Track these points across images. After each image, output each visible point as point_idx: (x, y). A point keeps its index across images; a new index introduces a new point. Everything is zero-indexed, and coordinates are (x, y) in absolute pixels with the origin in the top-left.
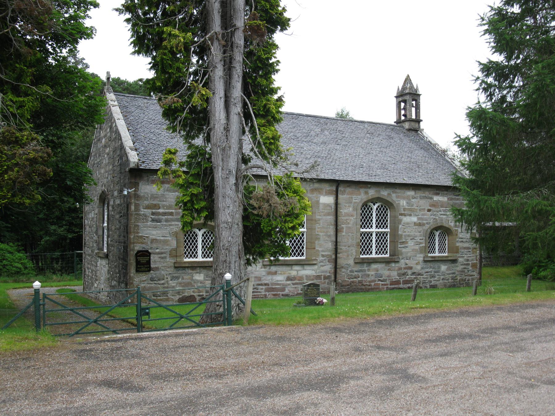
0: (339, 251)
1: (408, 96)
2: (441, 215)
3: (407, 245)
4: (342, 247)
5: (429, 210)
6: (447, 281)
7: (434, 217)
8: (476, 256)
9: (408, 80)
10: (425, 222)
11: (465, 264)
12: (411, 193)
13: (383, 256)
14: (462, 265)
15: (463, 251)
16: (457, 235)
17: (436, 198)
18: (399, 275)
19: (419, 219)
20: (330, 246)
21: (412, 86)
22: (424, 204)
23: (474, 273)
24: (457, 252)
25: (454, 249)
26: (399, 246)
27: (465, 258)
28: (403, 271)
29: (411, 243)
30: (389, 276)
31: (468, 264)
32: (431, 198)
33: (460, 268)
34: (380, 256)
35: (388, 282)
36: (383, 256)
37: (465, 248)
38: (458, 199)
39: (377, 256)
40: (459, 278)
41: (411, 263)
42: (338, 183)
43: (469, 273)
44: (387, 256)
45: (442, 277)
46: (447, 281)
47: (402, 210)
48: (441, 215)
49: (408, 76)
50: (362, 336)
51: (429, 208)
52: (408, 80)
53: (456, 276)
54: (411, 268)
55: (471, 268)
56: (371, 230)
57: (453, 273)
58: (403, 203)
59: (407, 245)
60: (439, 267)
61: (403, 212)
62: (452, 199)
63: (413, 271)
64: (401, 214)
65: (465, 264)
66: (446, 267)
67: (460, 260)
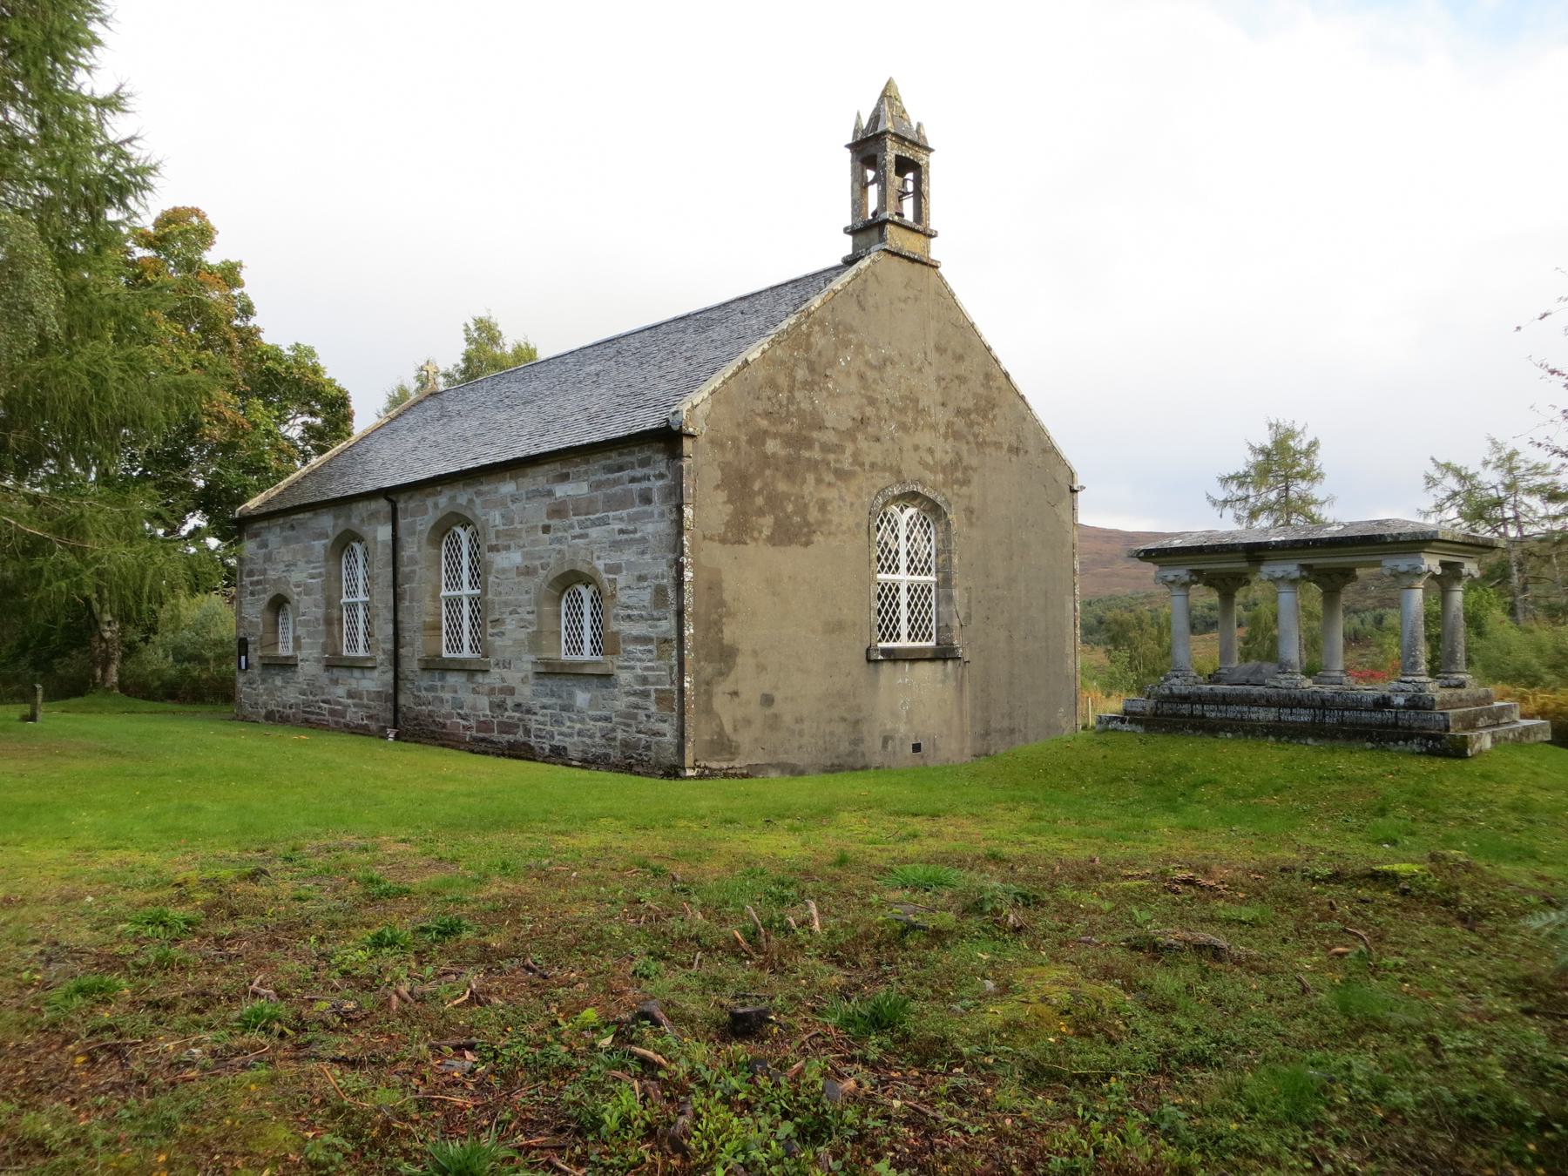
0: (402, 641)
1: (886, 153)
2: (574, 537)
3: (502, 629)
4: (406, 636)
5: (546, 529)
6: (588, 741)
7: (558, 547)
8: (671, 668)
9: (888, 95)
10: (537, 563)
11: (635, 694)
12: (508, 488)
13: (923, 644)
14: (628, 694)
15: (630, 648)
16: (613, 596)
17: (561, 491)
18: (492, 706)
19: (525, 556)
20: (390, 628)
21: (902, 115)
22: (536, 511)
23: (665, 727)
24: (615, 652)
25: (606, 643)
26: (490, 631)
27: (639, 672)
28: (497, 698)
29: (510, 624)
30: (474, 708)
31: (645, 694)
32: (550, 493)
33: (622, 703)
34: (917, 644)
35: (473, 723)
36: (923, 644)
37: (639, 640)
38: (616, 482)
39: (910, 644)
40: (620, 735)
41: (513, 677)
42: (390, 494)
43: (650, 725)
44: (932, 643)
45: (578, 726)
46: (588, 741)
47: (493, 536)
48: (574, 537)
49: (889, 84)
50: (1519, 868)
51: (547, 522)
52: (888, 95)
53: (614, 730)
54: (511, 691)
55: (653, 709)
56: (896, 577)
57: (607, 719)
58: (495, 517)
59: (502, 629)
60: (571, 695)
61: (494, 542)
62: (597, 486)
63: (517, 699)
64: (492, 549)
65: (635, 694)
66: (588, 696)
67: (624, 677)
